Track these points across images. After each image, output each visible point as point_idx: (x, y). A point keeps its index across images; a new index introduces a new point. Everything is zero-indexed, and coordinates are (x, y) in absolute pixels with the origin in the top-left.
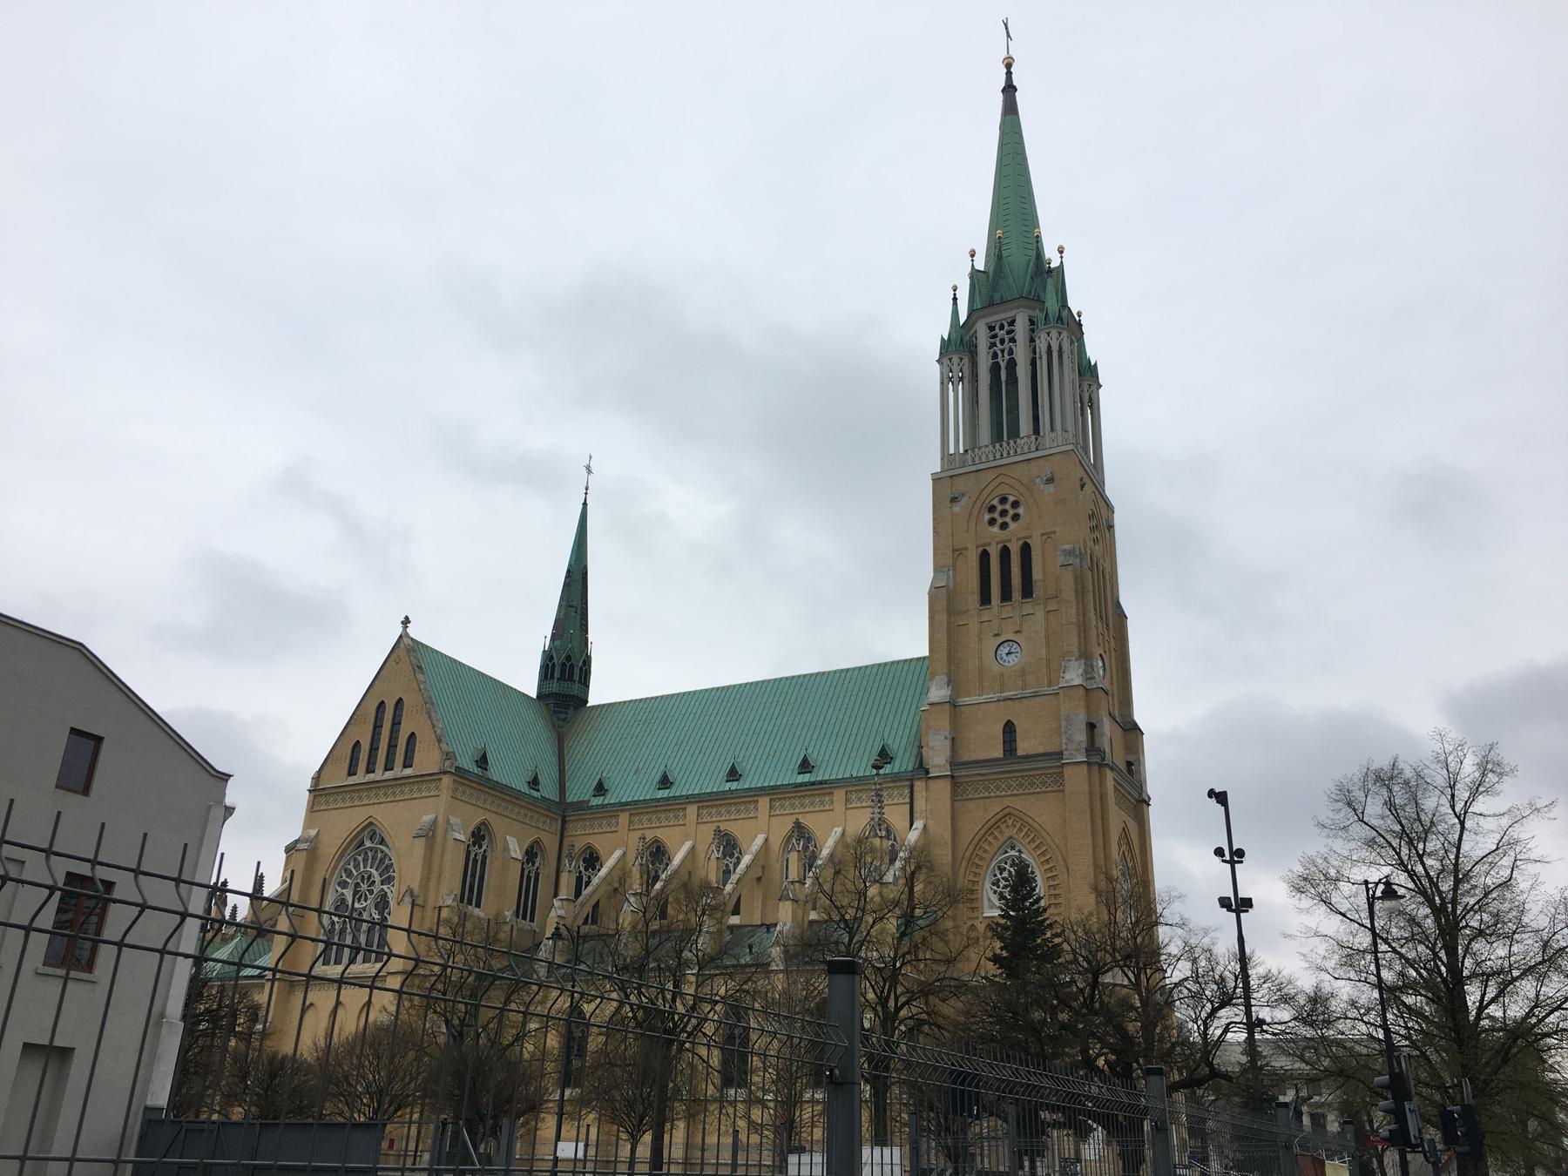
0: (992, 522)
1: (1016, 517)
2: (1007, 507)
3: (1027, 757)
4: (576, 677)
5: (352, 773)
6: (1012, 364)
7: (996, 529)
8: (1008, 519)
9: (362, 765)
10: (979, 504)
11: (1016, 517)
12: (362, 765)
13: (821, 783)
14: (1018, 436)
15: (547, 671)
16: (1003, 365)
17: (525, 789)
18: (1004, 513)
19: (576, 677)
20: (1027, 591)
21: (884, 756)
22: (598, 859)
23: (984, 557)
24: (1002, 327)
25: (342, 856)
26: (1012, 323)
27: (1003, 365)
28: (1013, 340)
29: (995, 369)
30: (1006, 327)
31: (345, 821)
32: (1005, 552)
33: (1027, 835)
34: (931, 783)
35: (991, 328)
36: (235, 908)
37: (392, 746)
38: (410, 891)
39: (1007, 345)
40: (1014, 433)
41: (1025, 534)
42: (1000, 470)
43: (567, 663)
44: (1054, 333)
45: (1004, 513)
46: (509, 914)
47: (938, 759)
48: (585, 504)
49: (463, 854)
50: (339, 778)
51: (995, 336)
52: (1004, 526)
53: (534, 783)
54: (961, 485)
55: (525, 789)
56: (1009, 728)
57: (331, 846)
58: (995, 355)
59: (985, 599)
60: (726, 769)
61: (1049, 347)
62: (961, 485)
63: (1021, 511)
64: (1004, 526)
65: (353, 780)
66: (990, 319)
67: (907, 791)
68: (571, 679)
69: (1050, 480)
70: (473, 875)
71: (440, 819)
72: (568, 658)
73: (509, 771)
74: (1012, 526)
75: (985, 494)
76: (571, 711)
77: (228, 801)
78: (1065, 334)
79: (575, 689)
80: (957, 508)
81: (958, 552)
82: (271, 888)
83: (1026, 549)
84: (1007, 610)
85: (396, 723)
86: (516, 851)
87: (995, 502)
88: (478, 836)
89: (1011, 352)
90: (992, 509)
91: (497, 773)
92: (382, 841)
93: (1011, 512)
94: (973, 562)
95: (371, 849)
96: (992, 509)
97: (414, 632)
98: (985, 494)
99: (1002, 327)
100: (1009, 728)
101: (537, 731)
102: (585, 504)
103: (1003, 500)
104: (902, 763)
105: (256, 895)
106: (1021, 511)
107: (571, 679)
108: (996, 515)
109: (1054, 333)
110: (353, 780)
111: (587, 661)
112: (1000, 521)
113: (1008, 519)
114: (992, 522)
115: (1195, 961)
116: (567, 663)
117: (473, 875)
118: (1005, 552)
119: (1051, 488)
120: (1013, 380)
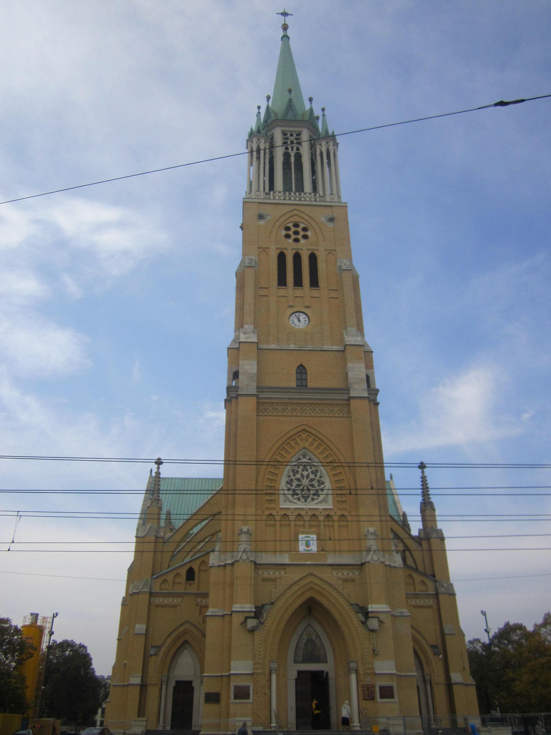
1: (305, 237)
6: (298, 157)
11: (305, 237)
14: (303, 191)
20: (314, 282)
23: (282, 257)
26: (299, 134)
29: (286, 156)
32: (297, 257)
33: (287, 452)
35: (284, 134)
36: (420, 591)
40: (300, 188)
44: (324, 143)
52: (296, 240)
56: (301, 370)
58: (287, 148)
59: (282, 281)
63: (309, 233)
64: (296, 240)
69: (331, 220)
77: (315, 115)
80: (262, 223)
83: (313, 258)
84: (298, 292)
87: (290, 225)
89: (298, 149)
90: (287, 229)
96: (287, 229)
100: (301, 370)
109: (324, 143)
113: (293, 237)
118: (297, 257)
119: (330, 225)
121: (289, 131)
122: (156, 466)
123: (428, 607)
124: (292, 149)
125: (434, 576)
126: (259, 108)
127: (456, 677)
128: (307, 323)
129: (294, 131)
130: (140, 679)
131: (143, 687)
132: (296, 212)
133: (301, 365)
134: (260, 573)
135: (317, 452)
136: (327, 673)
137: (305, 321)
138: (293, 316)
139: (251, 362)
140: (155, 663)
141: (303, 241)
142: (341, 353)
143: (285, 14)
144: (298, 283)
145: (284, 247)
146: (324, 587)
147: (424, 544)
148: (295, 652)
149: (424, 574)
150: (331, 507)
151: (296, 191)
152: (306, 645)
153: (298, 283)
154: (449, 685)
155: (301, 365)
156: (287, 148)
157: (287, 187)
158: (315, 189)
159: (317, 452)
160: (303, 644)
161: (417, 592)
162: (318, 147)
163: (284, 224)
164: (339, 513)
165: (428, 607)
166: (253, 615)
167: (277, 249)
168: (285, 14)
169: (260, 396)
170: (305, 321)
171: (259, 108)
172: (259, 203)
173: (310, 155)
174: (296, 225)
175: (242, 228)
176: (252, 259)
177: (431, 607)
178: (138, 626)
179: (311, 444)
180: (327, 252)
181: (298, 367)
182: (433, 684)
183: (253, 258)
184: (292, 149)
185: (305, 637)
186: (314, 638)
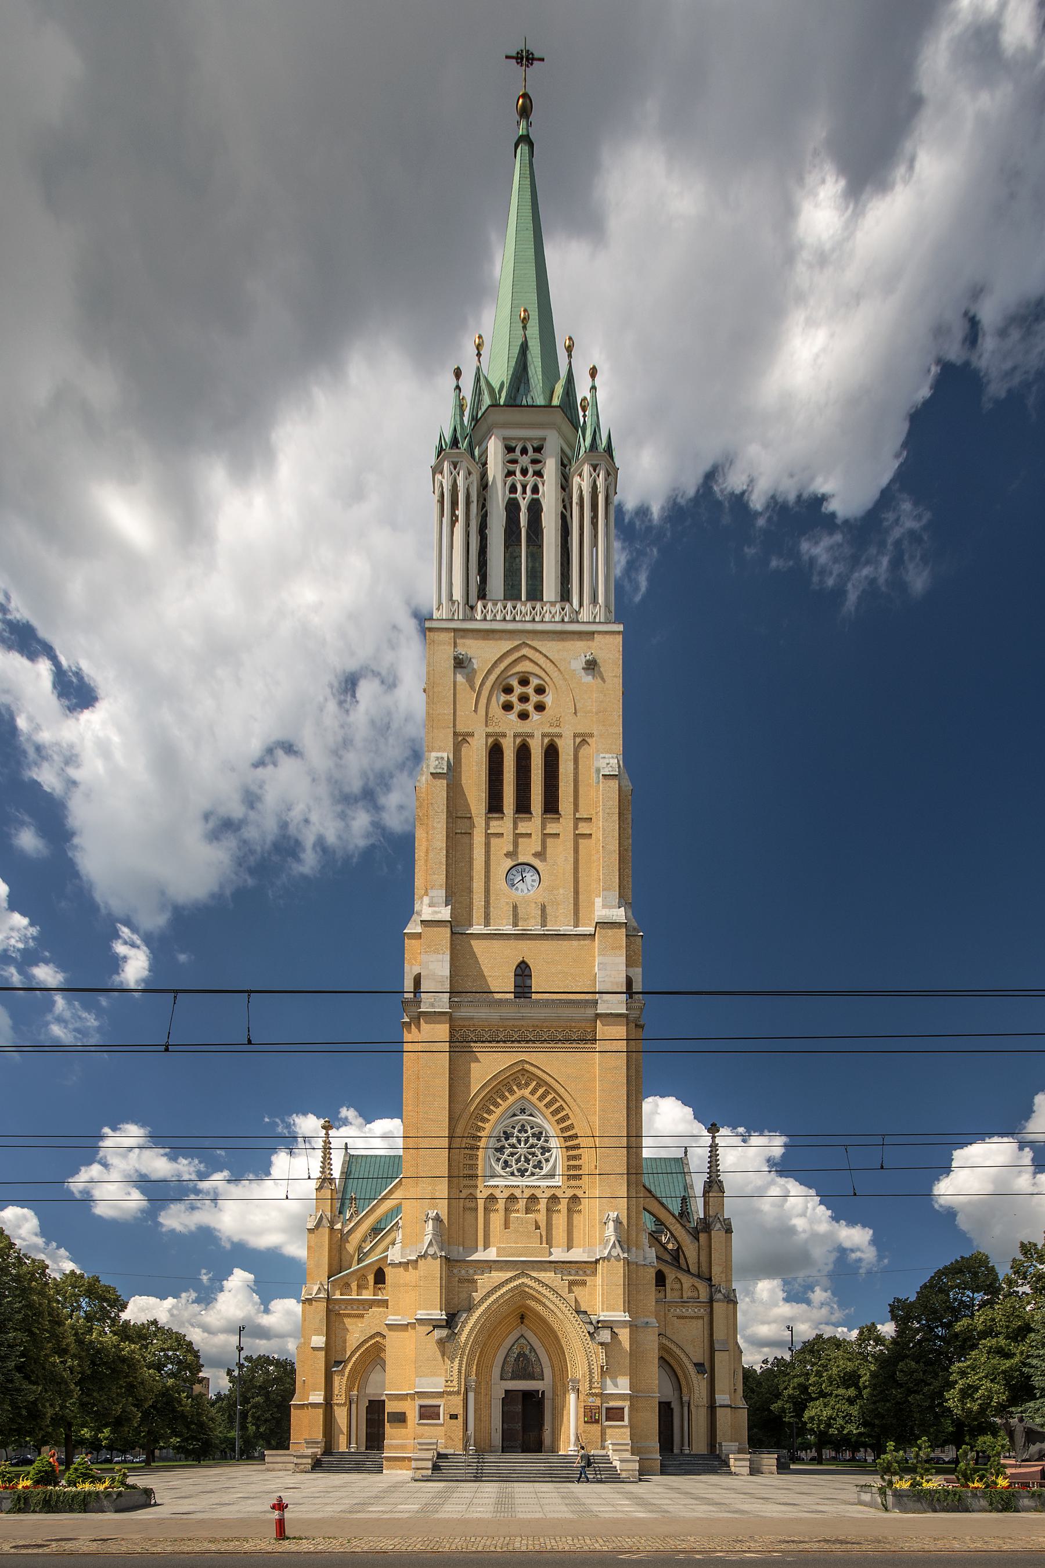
1: (540, 707)
6: (535, 508)
8: (530, 707)
9: (545, 1102)
10: (493, 678)
11: (540, 707)
12: (545, 1102)
16: (524, 505)
18: (524, 699)
23: (495, 753)
24: (535, 462)
26: (538, 450)
27: (524, 505)
28: (539, 474)
29: (512, 507)
32: (523, 753)
35: (510, 449)
40: (535, 594)
52: (524, 716)
56: (523, 971)
58: (513, 489)
61: (594, 487)
64: (524, 716)
69: (592, 666)
75: (502, 666)
83: (551, 753)
87: (534, 682)
89: (535, 490)
93: (530, 690)
94: (565, 803)
99: (524, 451)
113: (518, 707)
115: (68, 1437)
118: (523, 753)
119: (579, 664)
121: (520, 439)
122: (324, 1131)
123: (697, 1318)
124: (524, 492)
125: (710, 1279)
126: (458, 373)
127: (721, 1398)
128: (536, 884)
129: (530, 439)
130: (322, 1397)
131: (328, 1405)
132: (525, 651)
133: (523, 962)
134: (455, 1271)
135: (541, 1105)
136: (543, 1392)
137: (533, 881)
138: (513, 871)
139: (441, 956)
140: (340, 1383)
141: (535, 716)
143: (525, 58)
144: (523, 807)
145: (500, 730)
146: (540, 1289)
147: (703, 1237)
148: (503, 1368)
149: (699, 1276)
150: (560, 1184)
151: (528, 599)
152: (517, 1360)
153: (523, 807)
154: (712, 1408)
155: (523, 962)
156: (513, 489)
157: (512, 593)
158: (565, 595)
159: (541, 1105)
160: (513, 1359)
161: (685, 1299)
162: (576, 480)
163: (501, 679)
164: (570, 1193)
165: (697, 1318)
166: (444, 1323)
167: (488, 735)
168: (525, 58)
169: (457, 1015)
170: (533, 881)
171: (458, 373)
172: (455, 630)
173: (560, 508)
174: (524, 682)
175: (425, 691)
176: (442, 758)
177: (702, 1318)
178: (314, 1338)
179: (533, 1093)
180: (578, 740)
181: (518, 966)
182: (692, 1406)
183: (445, 755)
184: (524, 492)
185: (516, 1350)
186: (527, 1352)
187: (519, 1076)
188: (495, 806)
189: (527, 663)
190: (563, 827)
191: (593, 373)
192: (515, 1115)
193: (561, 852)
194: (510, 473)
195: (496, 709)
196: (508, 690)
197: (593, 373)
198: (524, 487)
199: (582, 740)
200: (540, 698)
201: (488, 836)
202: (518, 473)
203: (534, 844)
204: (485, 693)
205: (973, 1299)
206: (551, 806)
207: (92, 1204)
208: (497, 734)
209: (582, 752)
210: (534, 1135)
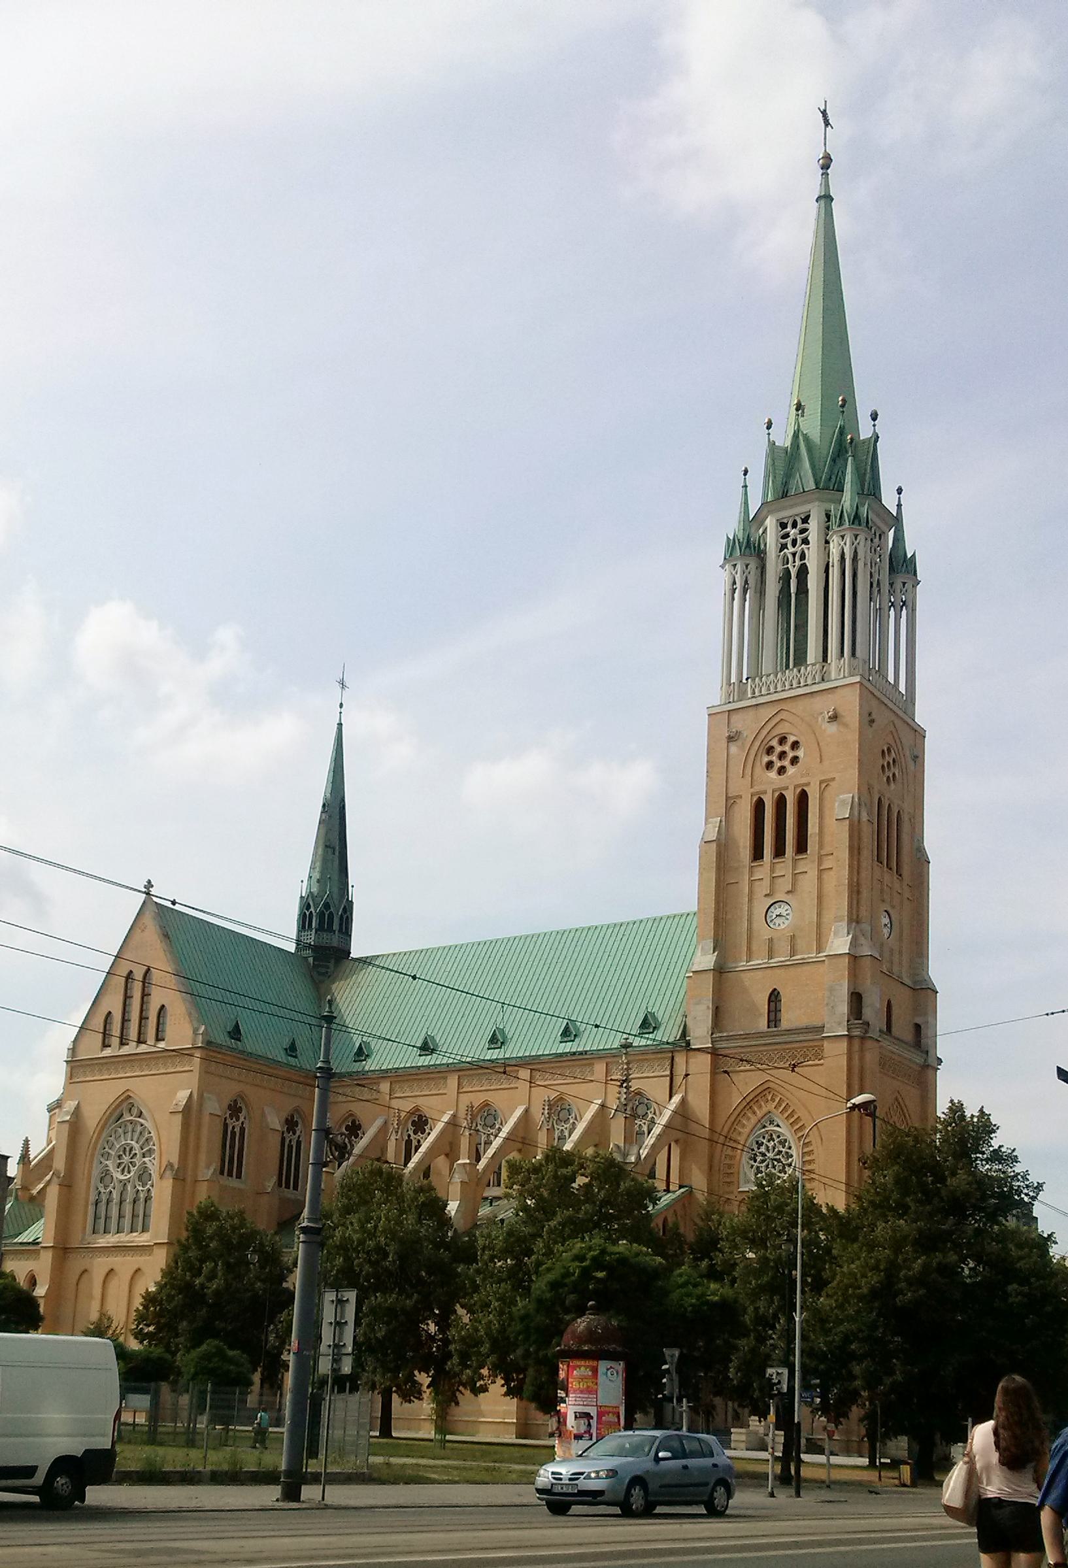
0: (770, 765)
2: (787, 748)
3: (789, 1031)
4: (336, 927)
5: (105, 1045)
6: (803, 571)
7: (773, 774)
9: (115, 1041)
10: (757, 744)
11: (794, 761)
13: (581, 1053)
15: (304, 922)
17: (281, 1057)
18: (782, 755)
19: (336, 927)
21: (648, 1024)
22: (359, 1127)
23: (759, 806)
24: (794, 525)
25: (103, 1128)
26: (805, 520)
28: (806, 541)
30: (800, 526)
31: (100, 1097)
32: (781, 802)
34: (691, 1053)
35: (783, 526)
37: (143, 1018)
38: (170, 1165)
39: (798, 549)
41: (804, 780)
42: (783, 706)
43: (328, 914)
45: (782, 755)
46: (270, 1184)
47: (701, 1036)
48: (340, 725)
49: (220, 1128)
50: (92, 1048)
51: (786, 536)
53: (292, 1050)
54: (738, 722)
55: (281, 1057)
57: (92, 1118)
60: (488, 1036)
62: (738, 722)
63: (800, 753)
64: (782, 770)
65: (108, 1052)
66: (785, 514)
67: (668, 1063)
68: (330, 929)
69: (834, 718)
70: (232, 1147)
71: (195, 1096)
72: (327, 906)
73: (266, 1039)
74: (791, 770)
75: (765, 732)
76: (331, 965)
78: (861, 538)
79: (335, 940)
80: (734, 749)
81: (730, 802)
82: (37, 1150)
83: (803, 798)
85: (145, 995)
86: (275, 1122)
87: (775, 743)
88: (234, 1110)
89: (803, 557)
91: (250, 1043)
92: (140, 1115)
93: (791, 754)
95: (131, 1122)
97: (163, 892)
98: (765, 732)
101: (296, 992)
102: (340, 725)
103: (782, 740)
104: (668, 1033)
105: (24, 1158)
106: (800, 753)
107: (330, 929)
108: (774, 758)
110: (108, 1052)
111: (348, 908)
112: (778, 764)
113: (786, 763)
114: (770, 765)
116: (328, 914)
117: (232, 1147)
118: (781, 802)
120: (803, 590)
142: (908, 992)
153: (779, 851)
174: (782, 740)
187: (763, 1093)
188: (758, 854)
189: (787, 724)
190: (808, 864)
191: (874, 417)
192: (765, 1127)
193: (808, 883)
194: (784, 547)
195: (759, 769)
196: (770, 751)
197: (874, 417)
198: (794, 555)
199: (825, 784)
200: (776, 768)
201: (751, 882)
202: (789, 546)
203: (785, 884)
204: (753, 753)
205: (419, 1221)
206: (801, 847)
207: (793, 1492)
208: (758, 793)
209: (826, 794)
210: (780, 1142)
